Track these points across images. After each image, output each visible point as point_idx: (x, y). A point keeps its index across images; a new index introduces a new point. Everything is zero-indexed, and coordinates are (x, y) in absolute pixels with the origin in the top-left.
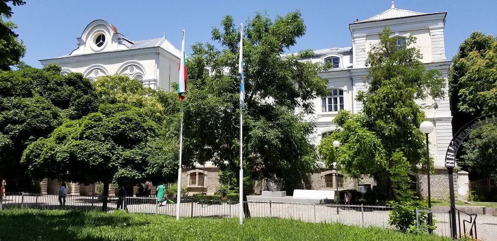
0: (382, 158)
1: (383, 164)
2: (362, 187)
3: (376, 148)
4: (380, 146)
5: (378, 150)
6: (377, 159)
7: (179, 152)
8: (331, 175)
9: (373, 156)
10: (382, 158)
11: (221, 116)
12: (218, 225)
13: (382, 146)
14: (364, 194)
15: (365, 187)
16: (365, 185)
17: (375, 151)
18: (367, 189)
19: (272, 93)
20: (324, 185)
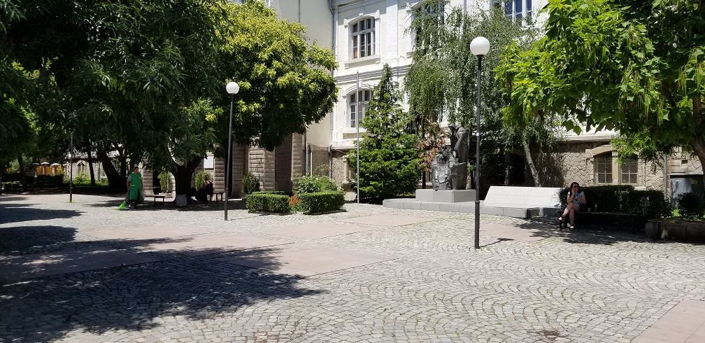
0: (644, 82)
1: (648, 102)
2: (680, 181)
3: (630, 55)
4: (642, 47)
5: (636, 60)
6: (624, 88)
7: (522, 148)
8: (609, 154)
9: (617, 77)
10: (644, 82)
11: (32, 161)
12: (444, 285)
13: (650, 47)
14: (225, 86)
15: (688, 183)
16: (687, 177)
17: (625, 64)
18: (693, 187)
19: (220, 86)
20: (592, 177)
